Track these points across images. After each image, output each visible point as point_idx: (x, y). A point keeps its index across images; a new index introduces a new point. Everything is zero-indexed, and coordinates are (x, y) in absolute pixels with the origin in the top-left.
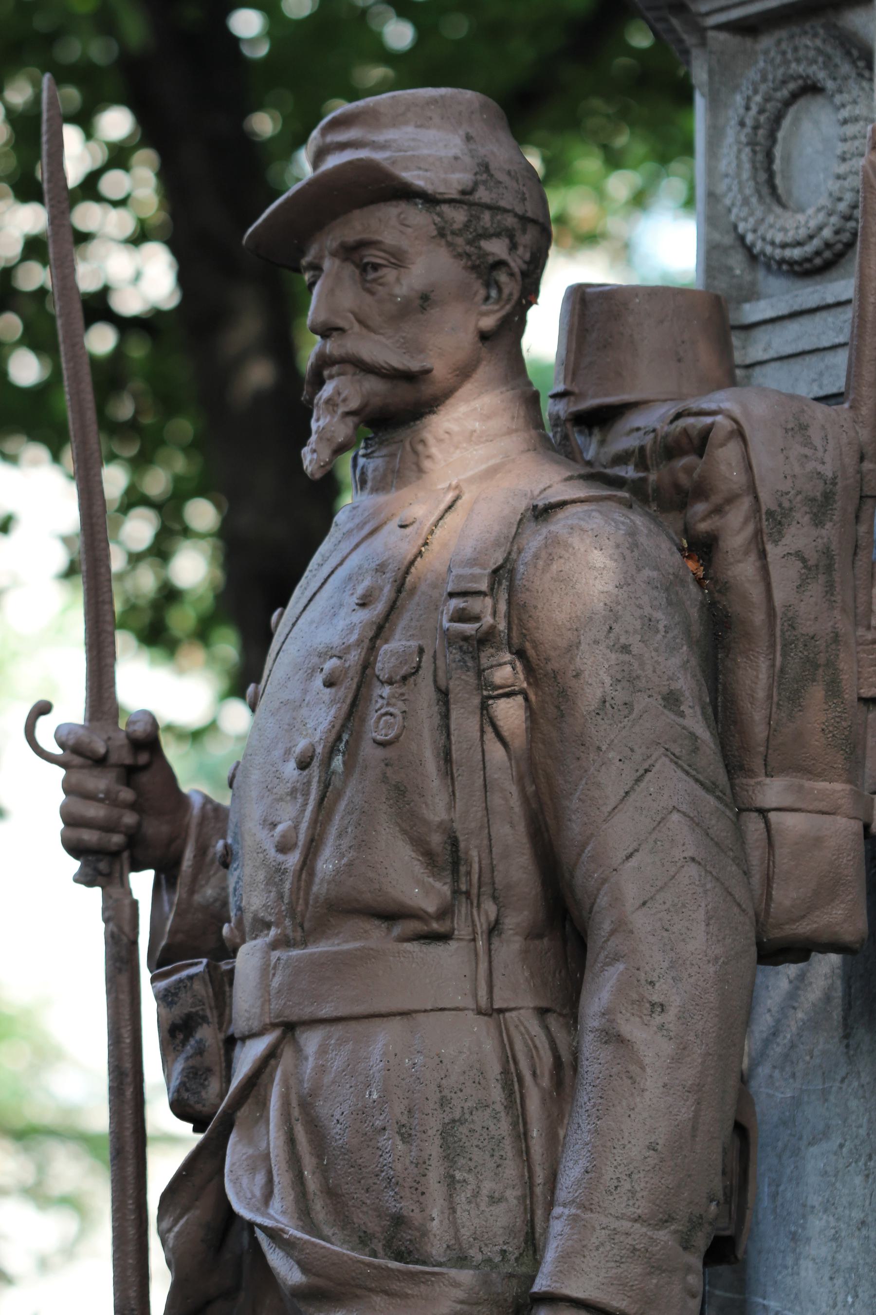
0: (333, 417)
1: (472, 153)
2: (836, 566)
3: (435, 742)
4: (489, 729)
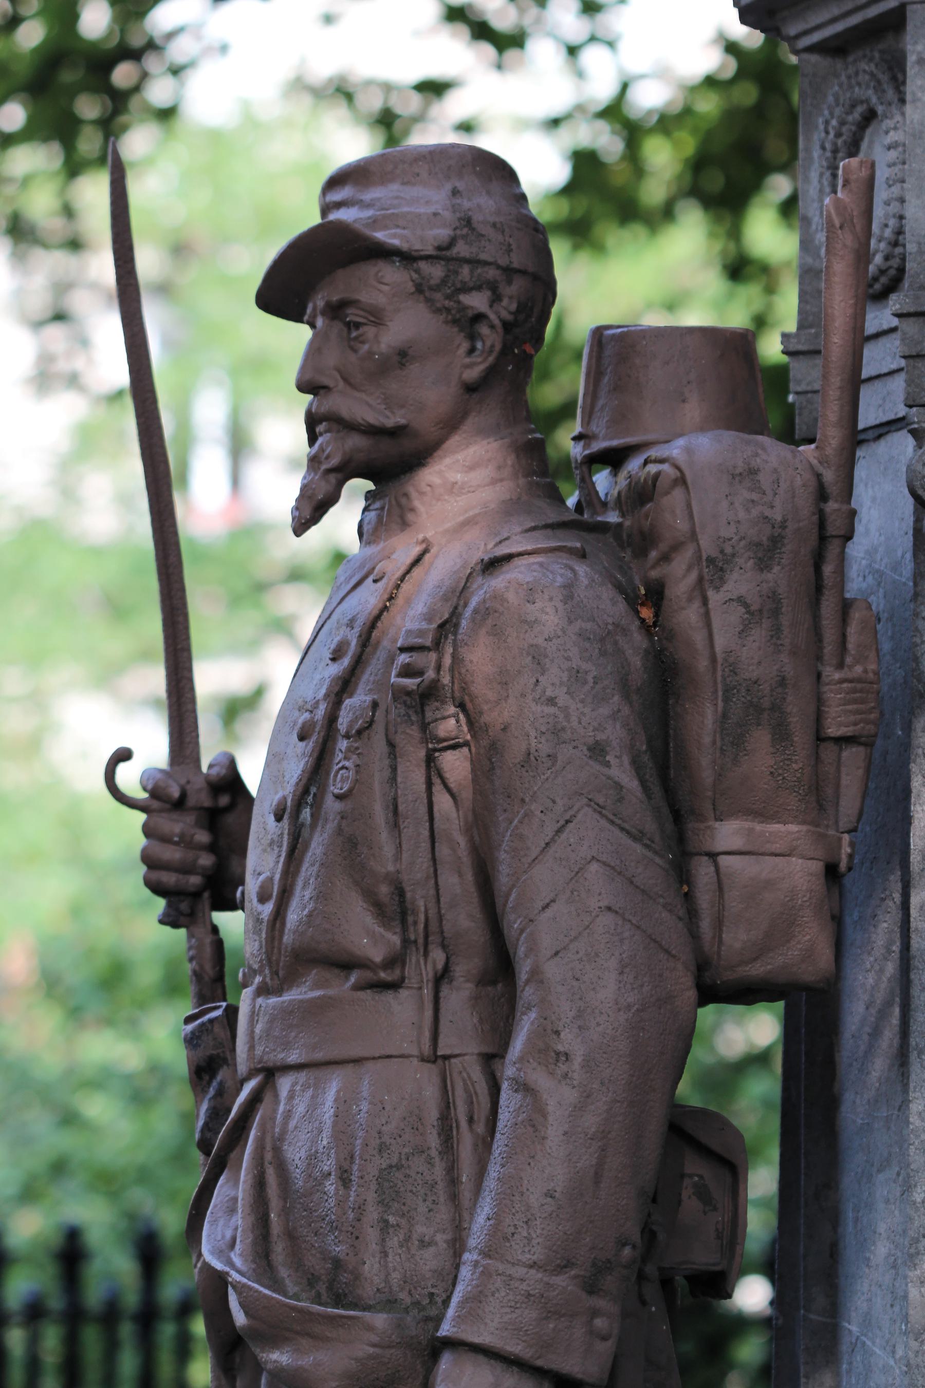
0: (316, 474)
1: (454, 209)
2: (783, 610)
3: (384, 795)
4: (436, 781)
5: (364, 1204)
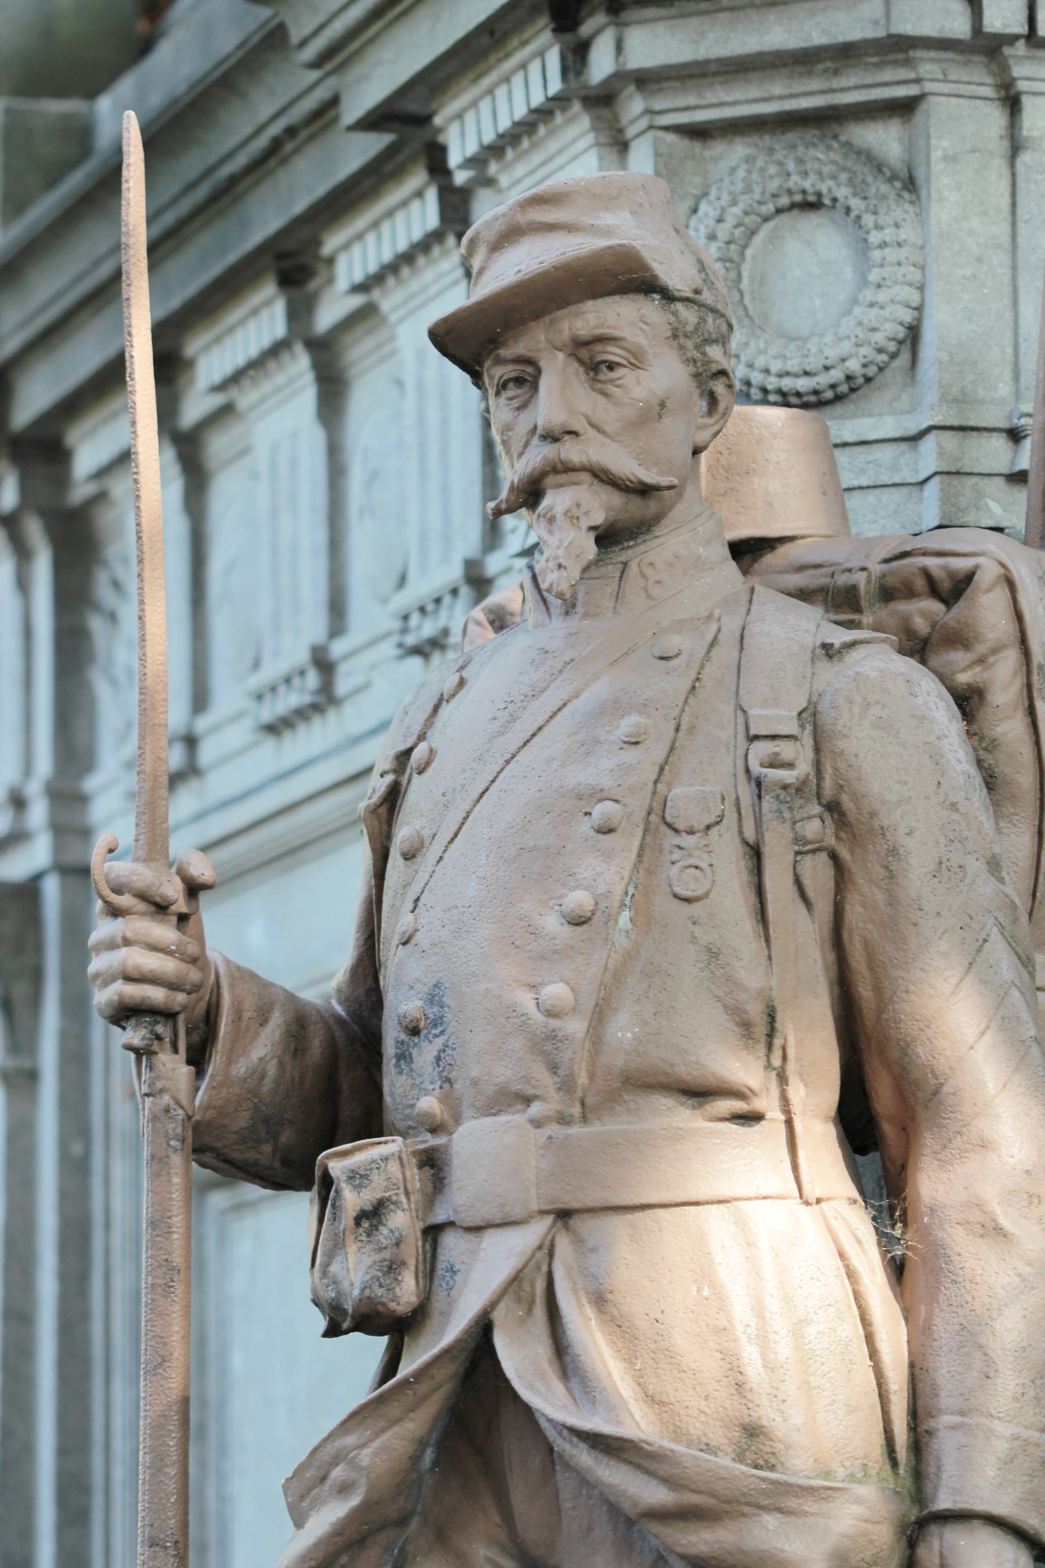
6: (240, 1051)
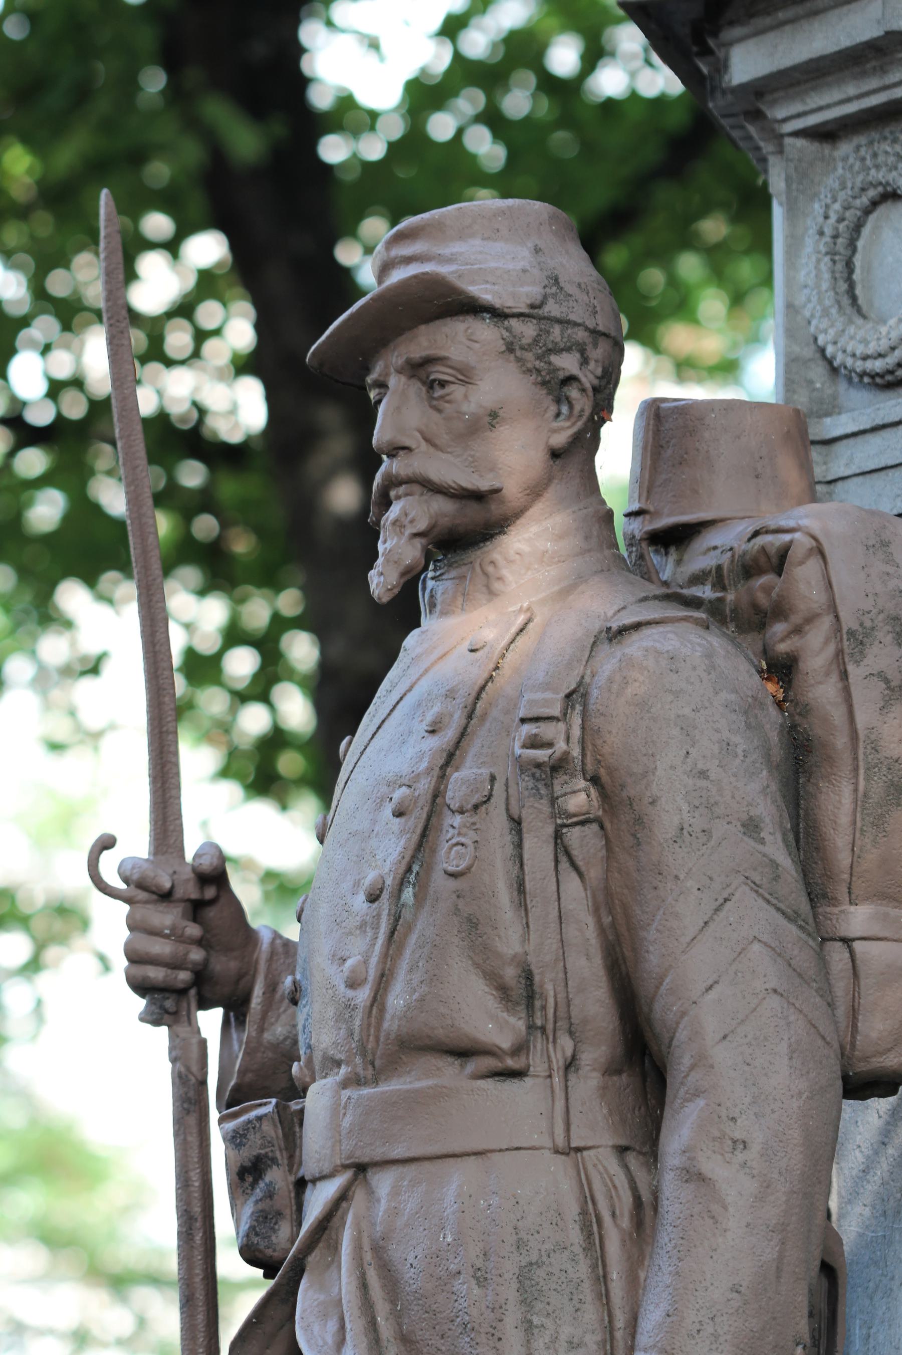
4: (563, 859)
5: (506, 1304)
6: (273, 1020)
